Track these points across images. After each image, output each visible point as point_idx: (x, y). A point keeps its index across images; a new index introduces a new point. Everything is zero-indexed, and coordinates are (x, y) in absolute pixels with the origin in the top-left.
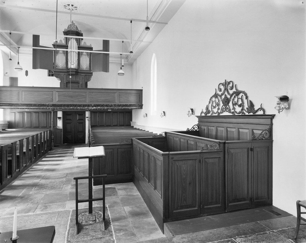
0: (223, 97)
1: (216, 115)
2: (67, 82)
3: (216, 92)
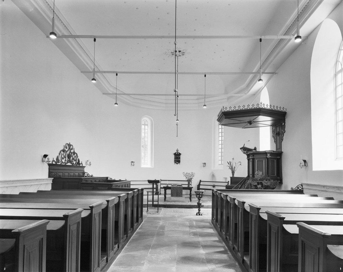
0: (68, 153)
1: (64, 164)
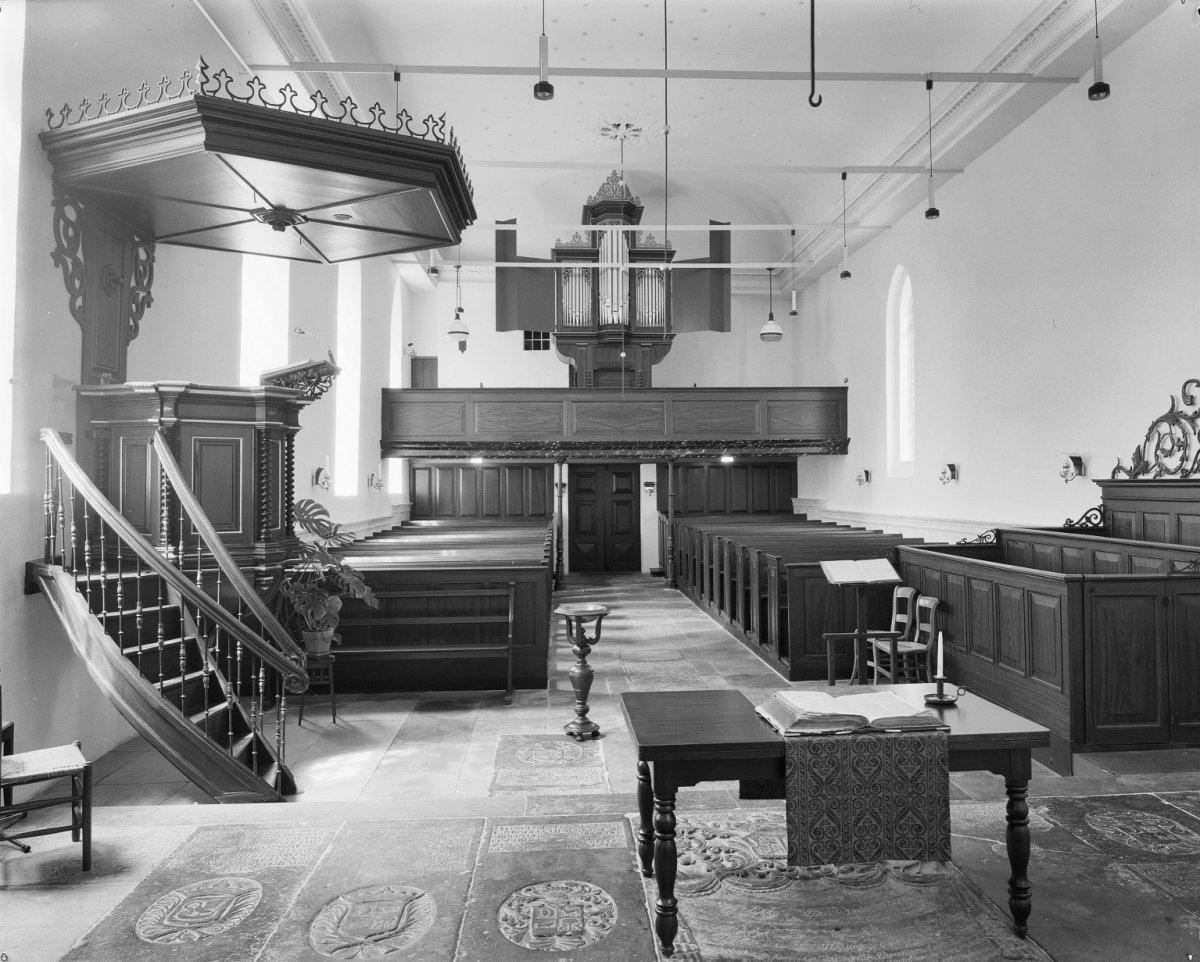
1: (1177, 477)
2: (597, 368)
3: (1173, 405)
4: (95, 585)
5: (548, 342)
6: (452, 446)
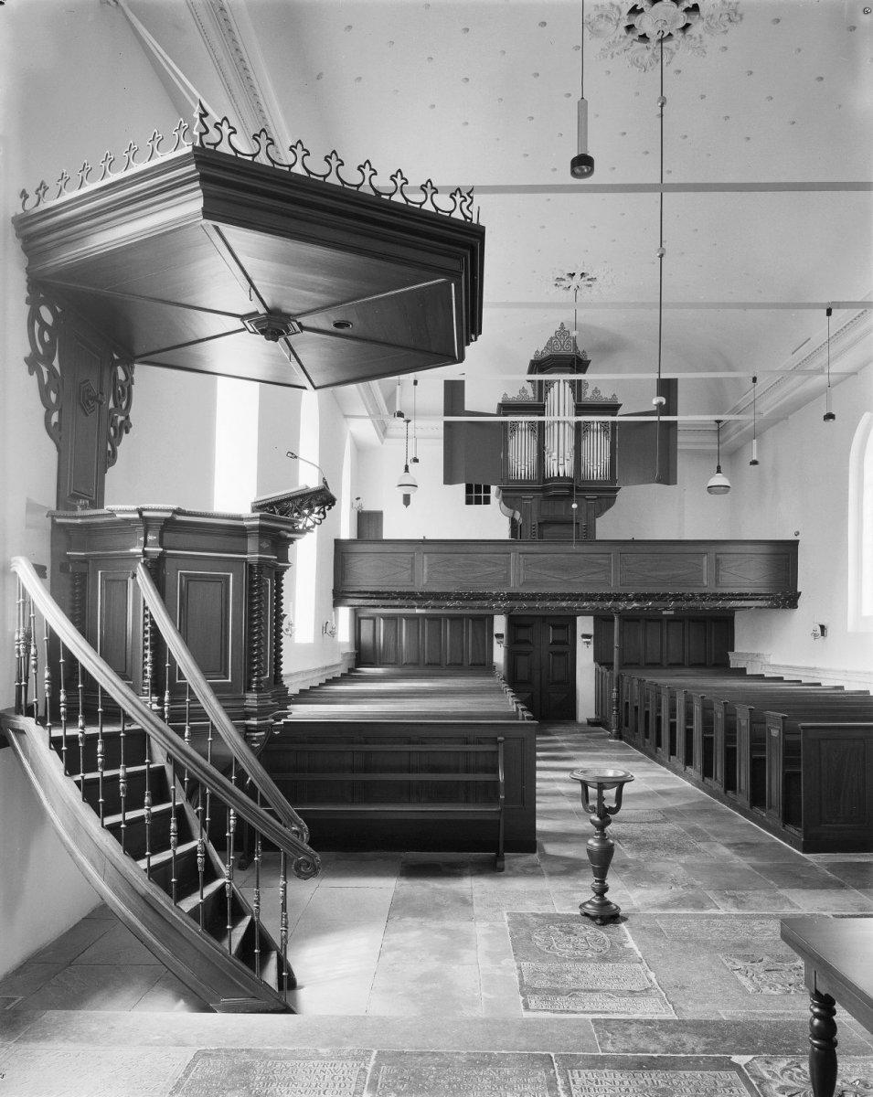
4: (72, 740)
5: (489, 497)
6: (401, 595)
